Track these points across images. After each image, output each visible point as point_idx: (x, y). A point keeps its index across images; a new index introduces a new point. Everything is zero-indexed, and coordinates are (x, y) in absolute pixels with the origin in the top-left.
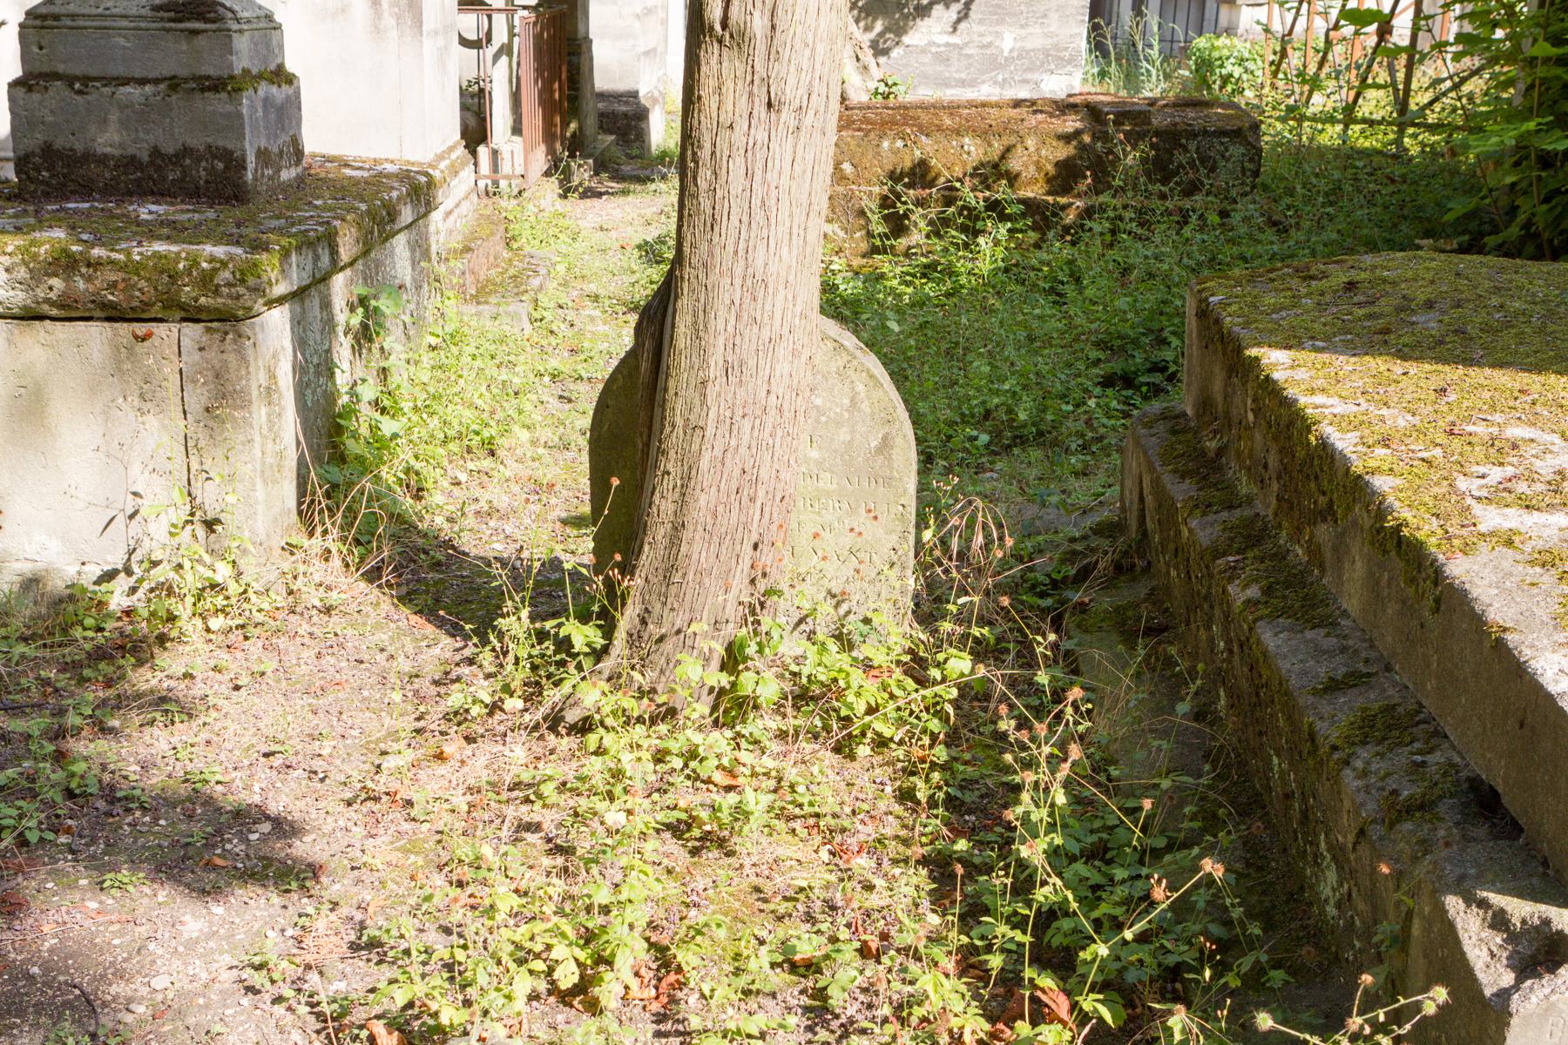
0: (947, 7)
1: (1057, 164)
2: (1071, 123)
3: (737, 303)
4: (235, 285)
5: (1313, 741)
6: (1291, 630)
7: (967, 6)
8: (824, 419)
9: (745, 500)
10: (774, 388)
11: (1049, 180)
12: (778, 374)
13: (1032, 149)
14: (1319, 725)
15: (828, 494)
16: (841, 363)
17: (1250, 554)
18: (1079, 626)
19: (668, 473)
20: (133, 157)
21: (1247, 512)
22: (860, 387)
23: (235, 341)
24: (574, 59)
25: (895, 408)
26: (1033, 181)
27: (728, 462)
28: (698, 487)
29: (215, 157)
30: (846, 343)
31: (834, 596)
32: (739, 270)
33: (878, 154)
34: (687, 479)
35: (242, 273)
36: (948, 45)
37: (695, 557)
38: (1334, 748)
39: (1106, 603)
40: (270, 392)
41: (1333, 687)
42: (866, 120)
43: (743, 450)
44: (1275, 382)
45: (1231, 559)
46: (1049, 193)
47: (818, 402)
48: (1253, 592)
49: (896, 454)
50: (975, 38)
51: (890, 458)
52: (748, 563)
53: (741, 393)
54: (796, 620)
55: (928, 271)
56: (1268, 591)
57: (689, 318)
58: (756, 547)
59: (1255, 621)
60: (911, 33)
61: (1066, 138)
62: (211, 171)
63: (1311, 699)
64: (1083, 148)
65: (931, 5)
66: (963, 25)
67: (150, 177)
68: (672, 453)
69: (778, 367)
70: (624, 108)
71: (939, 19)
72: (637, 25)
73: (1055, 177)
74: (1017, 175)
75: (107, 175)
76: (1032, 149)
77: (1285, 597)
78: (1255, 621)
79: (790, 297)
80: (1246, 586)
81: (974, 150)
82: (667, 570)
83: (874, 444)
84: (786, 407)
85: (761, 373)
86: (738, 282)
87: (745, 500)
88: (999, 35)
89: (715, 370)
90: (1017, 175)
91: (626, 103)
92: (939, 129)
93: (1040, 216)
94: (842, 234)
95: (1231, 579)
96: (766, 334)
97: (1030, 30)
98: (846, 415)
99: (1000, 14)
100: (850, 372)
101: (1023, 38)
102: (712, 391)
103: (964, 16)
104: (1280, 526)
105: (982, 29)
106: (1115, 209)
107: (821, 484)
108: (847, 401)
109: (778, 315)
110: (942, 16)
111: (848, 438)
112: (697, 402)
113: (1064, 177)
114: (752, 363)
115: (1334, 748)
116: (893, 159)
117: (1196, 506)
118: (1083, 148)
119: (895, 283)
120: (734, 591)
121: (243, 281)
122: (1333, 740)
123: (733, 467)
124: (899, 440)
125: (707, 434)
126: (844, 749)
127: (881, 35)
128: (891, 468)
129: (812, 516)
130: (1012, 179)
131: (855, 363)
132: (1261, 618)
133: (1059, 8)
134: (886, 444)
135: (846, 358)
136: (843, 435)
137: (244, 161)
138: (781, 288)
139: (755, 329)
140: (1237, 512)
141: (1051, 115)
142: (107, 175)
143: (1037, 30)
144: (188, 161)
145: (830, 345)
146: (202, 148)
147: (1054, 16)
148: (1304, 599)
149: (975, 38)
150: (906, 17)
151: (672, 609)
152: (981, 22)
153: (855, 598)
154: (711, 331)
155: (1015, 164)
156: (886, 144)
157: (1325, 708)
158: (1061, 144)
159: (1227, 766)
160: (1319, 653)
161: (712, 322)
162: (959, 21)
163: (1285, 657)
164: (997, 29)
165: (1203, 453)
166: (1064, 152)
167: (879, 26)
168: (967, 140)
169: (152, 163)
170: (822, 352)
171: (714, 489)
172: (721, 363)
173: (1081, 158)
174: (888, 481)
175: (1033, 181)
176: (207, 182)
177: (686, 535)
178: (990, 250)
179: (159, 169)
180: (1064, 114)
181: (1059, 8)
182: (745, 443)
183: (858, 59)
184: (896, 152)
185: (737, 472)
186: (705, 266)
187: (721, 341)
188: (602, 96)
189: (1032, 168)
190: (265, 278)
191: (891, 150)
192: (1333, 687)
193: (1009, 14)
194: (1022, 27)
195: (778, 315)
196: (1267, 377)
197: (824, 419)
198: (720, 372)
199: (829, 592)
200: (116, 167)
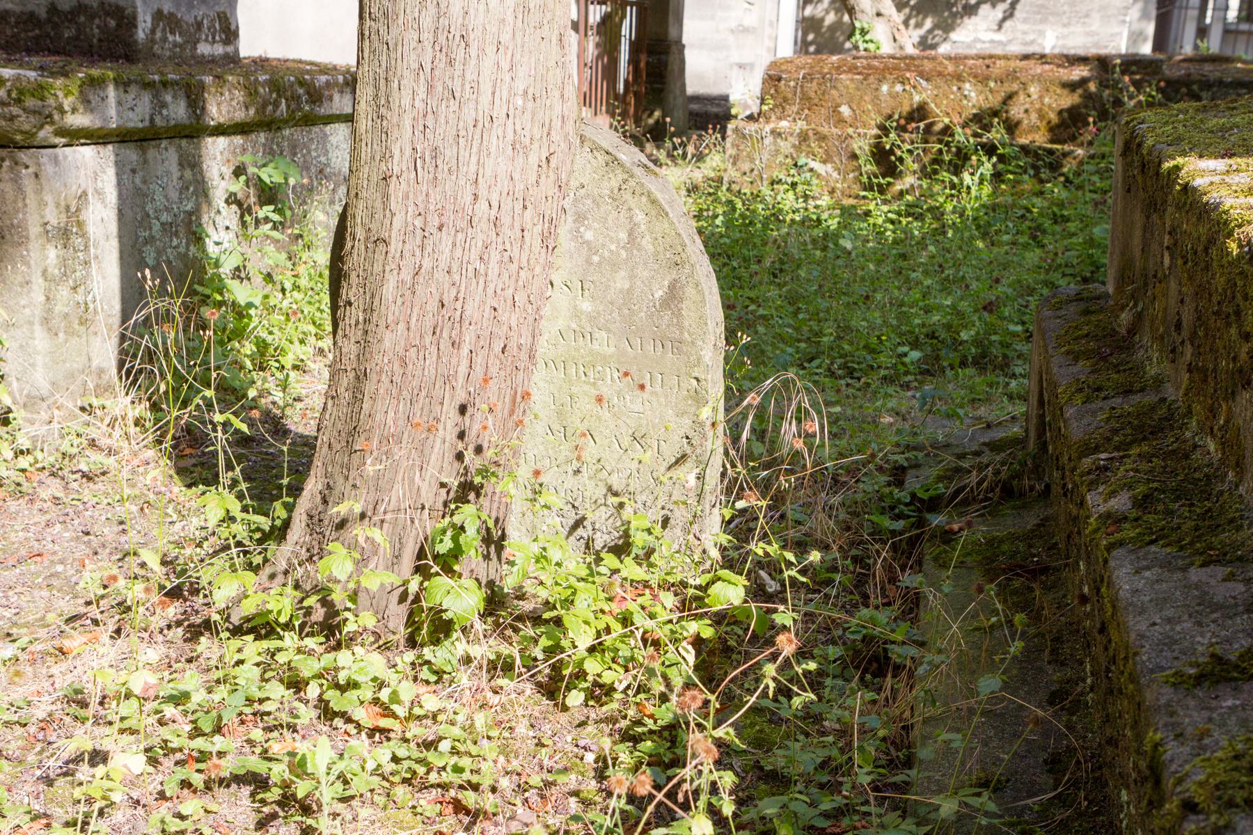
0: (994, 6)
1: (1060, 113)
2: (1078, 73)
3: (428, 68)
4: (9, 104)
5: (1158, 782)
6: (1166, 565)
7: (1013, 6)
8: (596, 259)
9: (445, 345)
10: (483, 193)
11: (1051, 130)
12: (488, 172)
13: (1035, 96)
14: (1172, 749)
15: (604, 359)
16: (615, 183)
17: (1134, 451)
18: (936, 559)
19: (350, 304)
20: (32, 14)
21: (1150, 398)
22: (640, 217)
23: (11, 169)
24: (663, 57)
25: (684, 246)
26: (1034, 129)
27: (419, 289)
28: (382, 324)
29: (108, 14)
30: (622, 157)
32: (427, 21)
33: (877, 97)
34: (369, 310)
35: (21, 92)
36: (992, 41)
37: (379, 417)
38: (1190, 807)
39: (981, 531)
40: (68, 232)
41: (1218, 673)
42: (869, 67)
43: (440, 275)
44: (1195, 189)
45: (1103, 456)
46: (1052, 141)
47: (589, 235)
48: (1121, 503)
49: (688, 310)
50: (1019, 35)
51: (678, 314)
52: (451, 435)
53: (435, 196)
54: (571, 522)
55: (913, 212)
56: (1144, 503)
57: (370, 91)
58: (463, 410)
59: (1110, 547)
60: (958, 30)
61: (1072, 86)
62: (104, 29)
63: (1167, 694)
64: (1088, 96)
65: (978, 5)
66: (1008, 24)
67: (48, 35)
68: (353, 275)
69: (489, 163)
70: (715, 110)
71: (985, 17)
72: (731, 38)
73: (1058, 126)
74: (1018, 123)
75: (9, 32)
76: (1035, 96)
77: (1170, 513)
78: (1110, 547)
79: (505, 65)
80: (1113, 494)
81: (974, 97)
82: (350, 434)
83: (659, 294)
84: (506, 220)
85: (463, 169)
86: (427, 36)
87: (445, 345)
88: (1042, 33)
89: (399, 163)
90: (1018, 123)
91: (718, 105)
92: (940, 74)
93: (1043, 163)
94: (835, 175)
95: (1092, 485)
96: (469, 114)
97: (1072, 29)
98: (624, 254)
99: (1044, 14)
100: (627, 196)
101: (1064, 37)
102: (397, 190)
103: (1009, 15)
104: (1189, 413)
105: (1025, 27)
107: (596, 346)
108: (623, 236)
109: (486, 88)
110: (989, 15)
112: (378, 204)
113: (1068, 125)
114: (450, 153)
115: (1190, 807)
116: (892, 103)
117: (1080, 390)
118: (1088, 96)
119: (880, 221)
120: (431, 470)
121: (19, 101)
122: (1191, 788)
123: (428, 294)
124: (690, 291)
125: (392, 248)
126: (552, 689)
127: (930, 31)
128: (681, 328)
129: (586, 388)
130: (1012, 127)
131: (632, 183)
132: (1121, 543)
133: (1102, 8)
134: (673, 295)
135: (621, 176)
136: (621, 281)
137: (135, 18)
138: (491, 49)
139: (454, 106)
140: (1136, 398)
141: (1059, 66)
142: (9, 32)
143: (1079, 29)
144: (82, 19)
145: (601, 158)
146: (95, 5)
147: (1096, 16)
148: (1202, 517)
149: (1019, 35)
150: (954, 16)
151: (354, 486)
152: (1025, 21)
154: (395, 106)
155: (1016, 111)
156: (885, 88)
157: (1192, 717)
158: (1066, 92)
159: (1075, 784)
160: (1205, 607)
161: (395, 94)
162: (1004, 19)
163: (1143, 611)
164: (1040, 27)
165: (1114, 333)
166: (1068, 100)
167: (928, 24)
168: (967, 86)
169: (49, 20)
170: (585, 168)
171: (402, 326)
172: (408, 151)
173: (1086, 107)
174: (678, 345)
175: (1034, 129)
176: (100, 40)
177: (369, 387)
178: (976, 183)
179: (55, 26)
180: (1073, 64)
181: (1102, 8)
182: (443, 265)
183: (895, 40)
184: (894, 96)
185: (433, 305)
186: (386, 15)
187: (407, 122)
188: (696, 98)
189: (1034, 116)
190: (51, 101)
191: (890, 94)
192: (1218, 673)
193: (1053, 14)
194: (1065, 26)
195: (486, 88)
196: (1186, 187)
197: (596, 259)
198: (406, 163)
199: (610, 489)
200: (17, 23)
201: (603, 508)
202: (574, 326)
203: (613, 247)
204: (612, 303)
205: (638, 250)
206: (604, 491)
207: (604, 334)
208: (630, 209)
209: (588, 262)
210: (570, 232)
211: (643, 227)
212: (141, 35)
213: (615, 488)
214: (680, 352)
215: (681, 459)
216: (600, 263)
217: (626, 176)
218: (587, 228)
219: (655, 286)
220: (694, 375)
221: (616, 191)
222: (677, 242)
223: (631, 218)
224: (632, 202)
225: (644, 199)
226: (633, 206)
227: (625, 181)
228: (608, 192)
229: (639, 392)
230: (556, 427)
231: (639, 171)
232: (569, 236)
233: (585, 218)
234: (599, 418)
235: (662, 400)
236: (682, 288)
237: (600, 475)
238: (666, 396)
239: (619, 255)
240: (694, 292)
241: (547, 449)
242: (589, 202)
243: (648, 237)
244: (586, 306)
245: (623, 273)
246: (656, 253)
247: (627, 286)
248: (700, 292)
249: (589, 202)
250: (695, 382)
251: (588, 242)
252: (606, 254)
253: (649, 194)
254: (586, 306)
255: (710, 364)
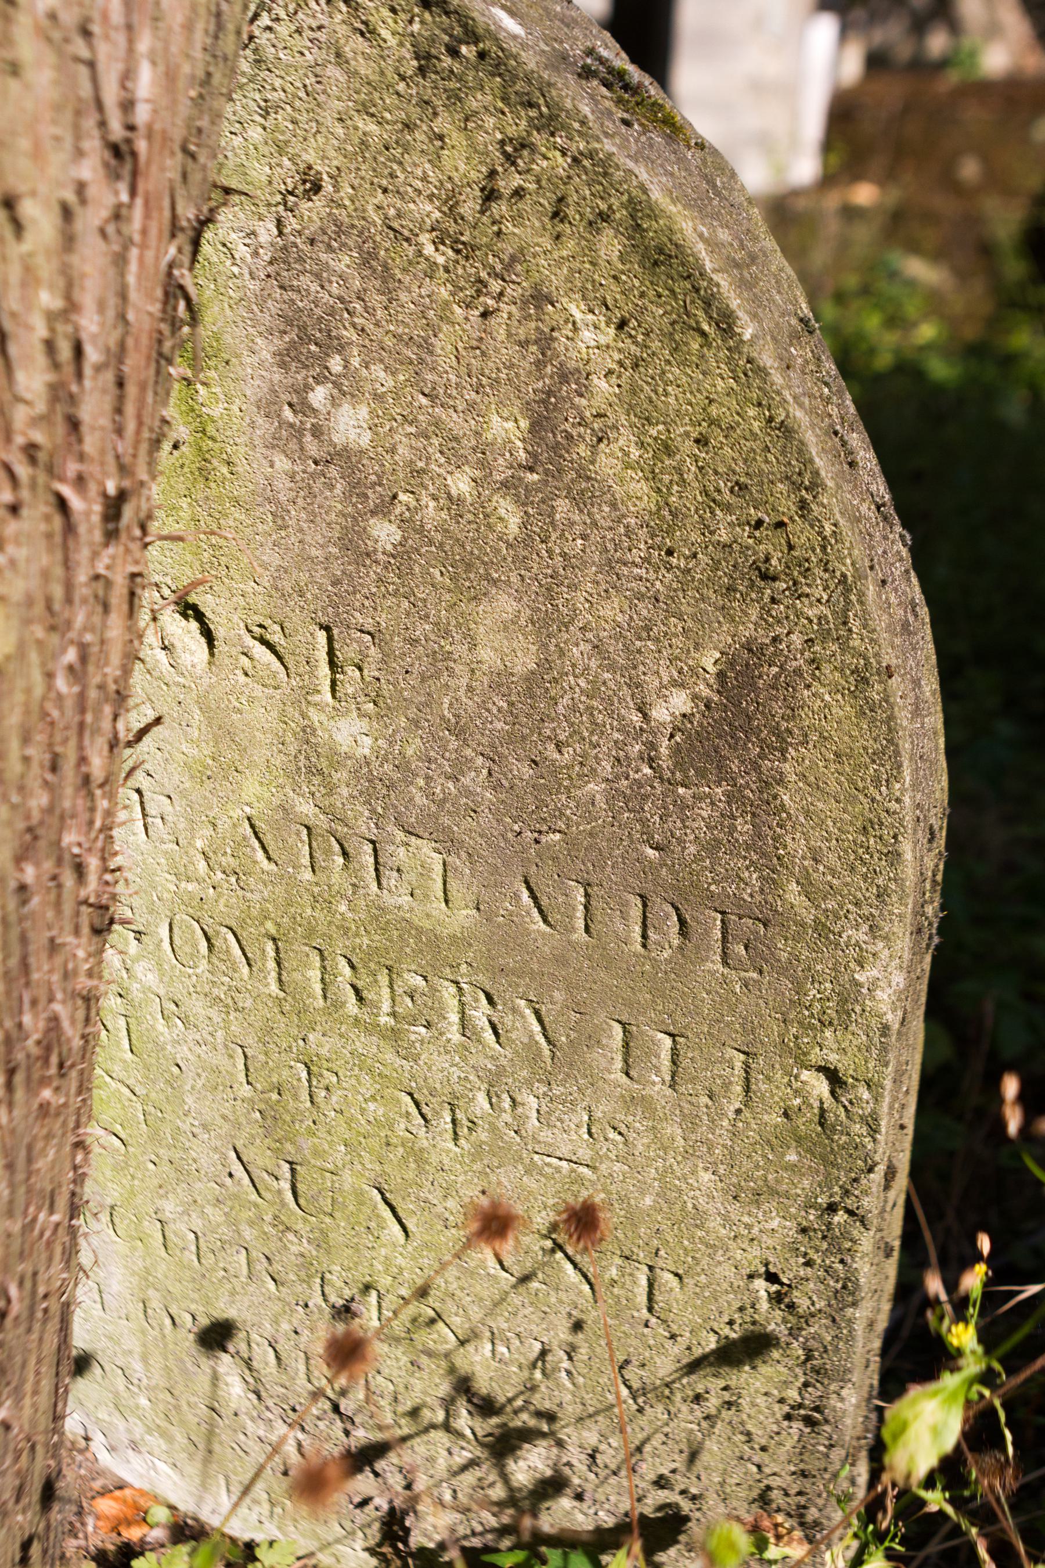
15: (436, 952)
16: (462, 165)
22: (589, 337)
25: (806, 486)
31: (486, 1407)
47: (351, 425)
49: (811, 795)
51: (762, 803)
98: (510, 517)
100: (527, 231)
106: (51, 971)
108: (506, 428)
111: (525, 661)
124: (825, 703)
128: (772, 864)
129: (365, 1044)
134: (741, 721)
136: (497, 639)
153: (578, 1438)
174: (753, 931)
197: (385, 533)
201: (439, 1436)
202: (306, 808)
203: (461, 484)
204: (459, 731)
205: (579, 501)
206: (444, 1388)
207: (426, 848)
208: (540, 298)
209: (353, 545)
210: (268, 407)
211: (601, 385)
212: (849, 396)
213: (483, 1385)
214: (759, 956)
215: (748, 1348)
216: (402, 554)
217: (517, 125)
218: (345, 390)
219: (658, 671)
220: (816, 1056)
221: (469, 207)
222: (771, 464)
223: (545, 341)
224: (551, 261)
225: (610, 245)
226: (555, 281)
227: (514, 151)
228: (430, 211)
229: (609, 1219)
230: (260, 1157)
231: (583, 101)
232: (265, 427)
233: (333, 344)
234: (420, 1157)
235: (673, 1130)
236: (788, 683)
237: (426, 1338)
238: (691, 1122)
239: (487, 516)
240: (843, 709)
241: (234, 1223)
242: (343, 262)
243: (625, 439)
244: (351, 734)
245: (505, 605)
246: (665, 521)
247: (525, 662)
248: (876, 713)
249: (343, 262)
250: (821, 1087)
251: (343, 457)
252: (431, 512)
253: (639, 211)
254: (351, 734)
255: (893, 1019)
